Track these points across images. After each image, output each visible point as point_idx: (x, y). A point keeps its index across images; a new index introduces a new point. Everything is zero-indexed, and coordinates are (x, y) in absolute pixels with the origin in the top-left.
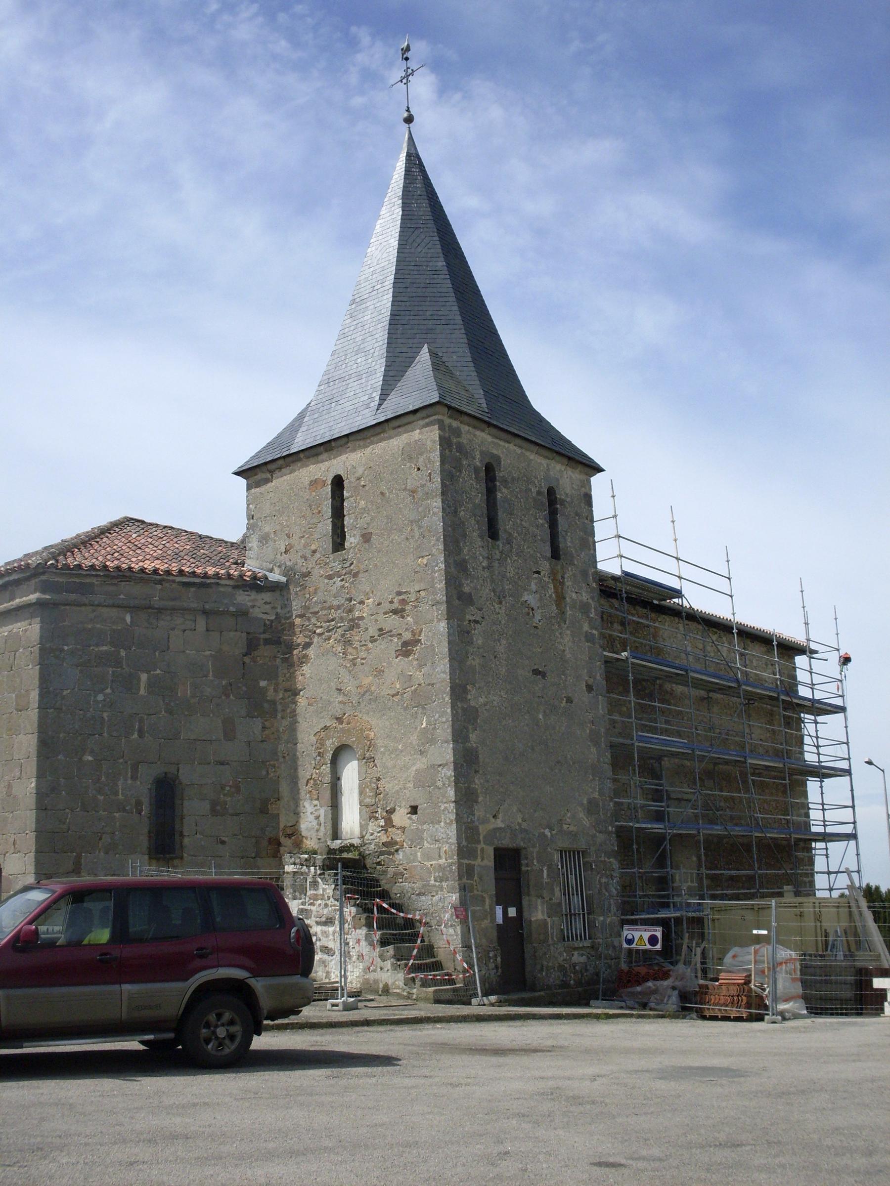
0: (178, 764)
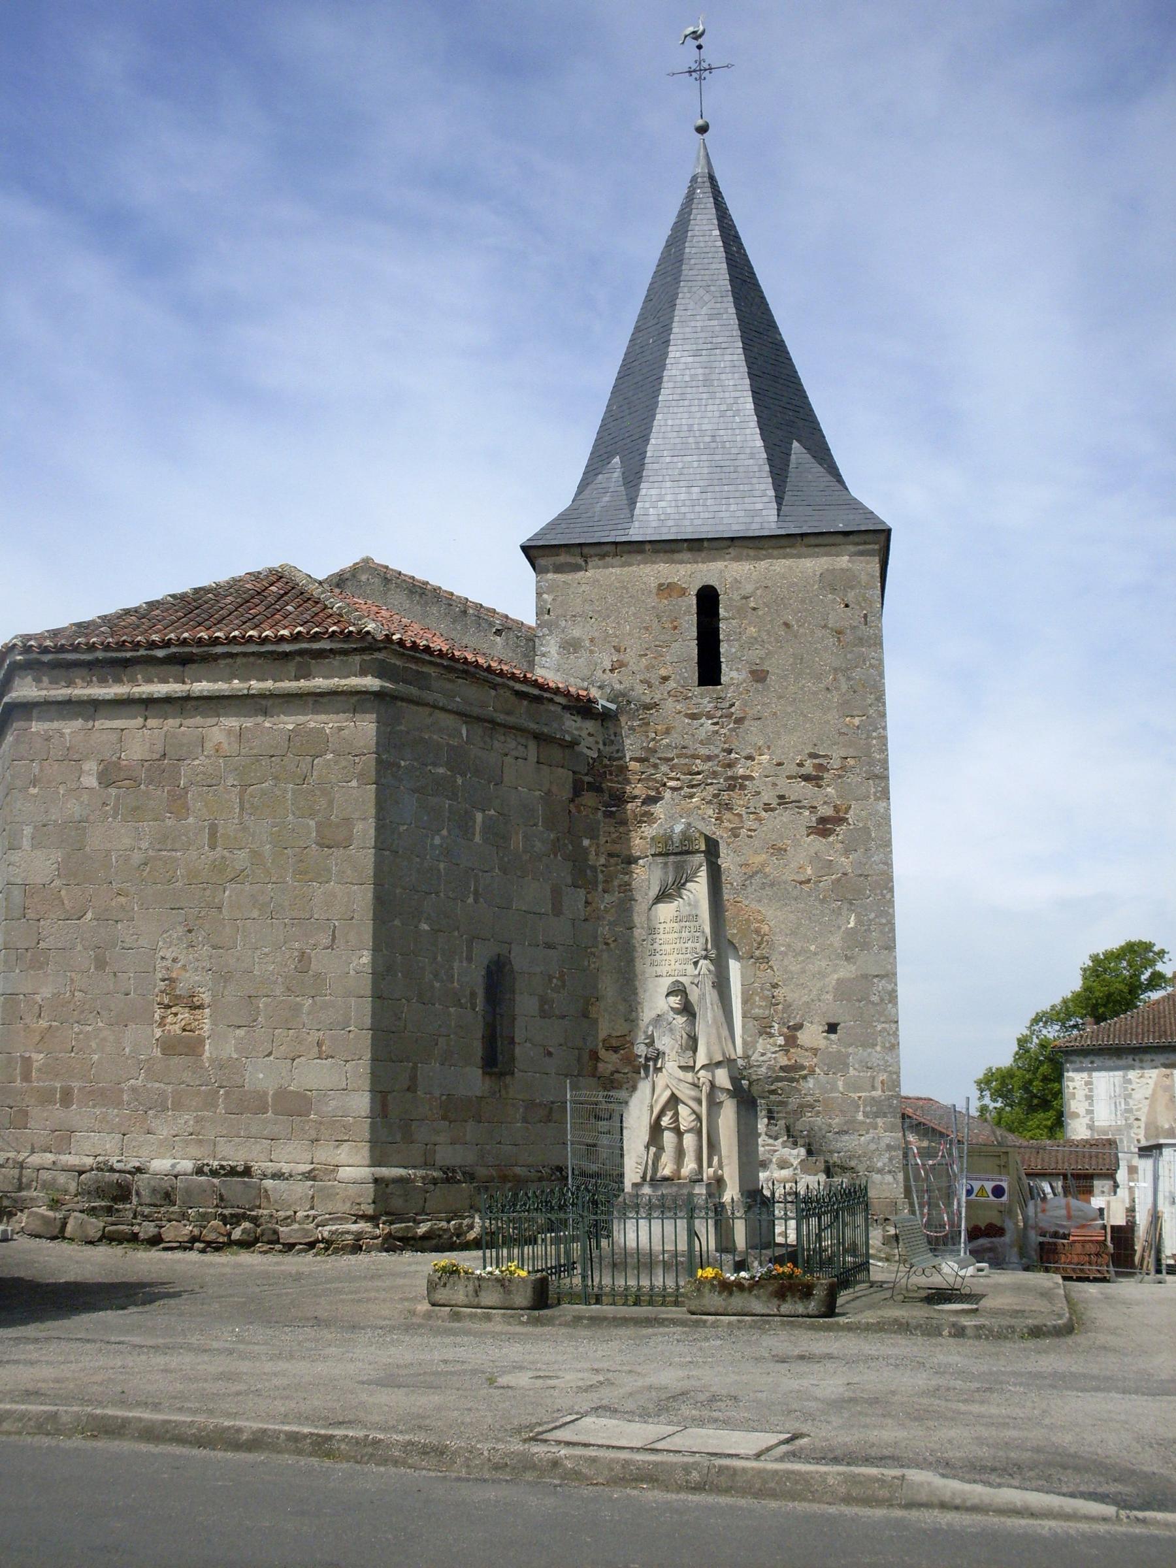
0: (510, 944)
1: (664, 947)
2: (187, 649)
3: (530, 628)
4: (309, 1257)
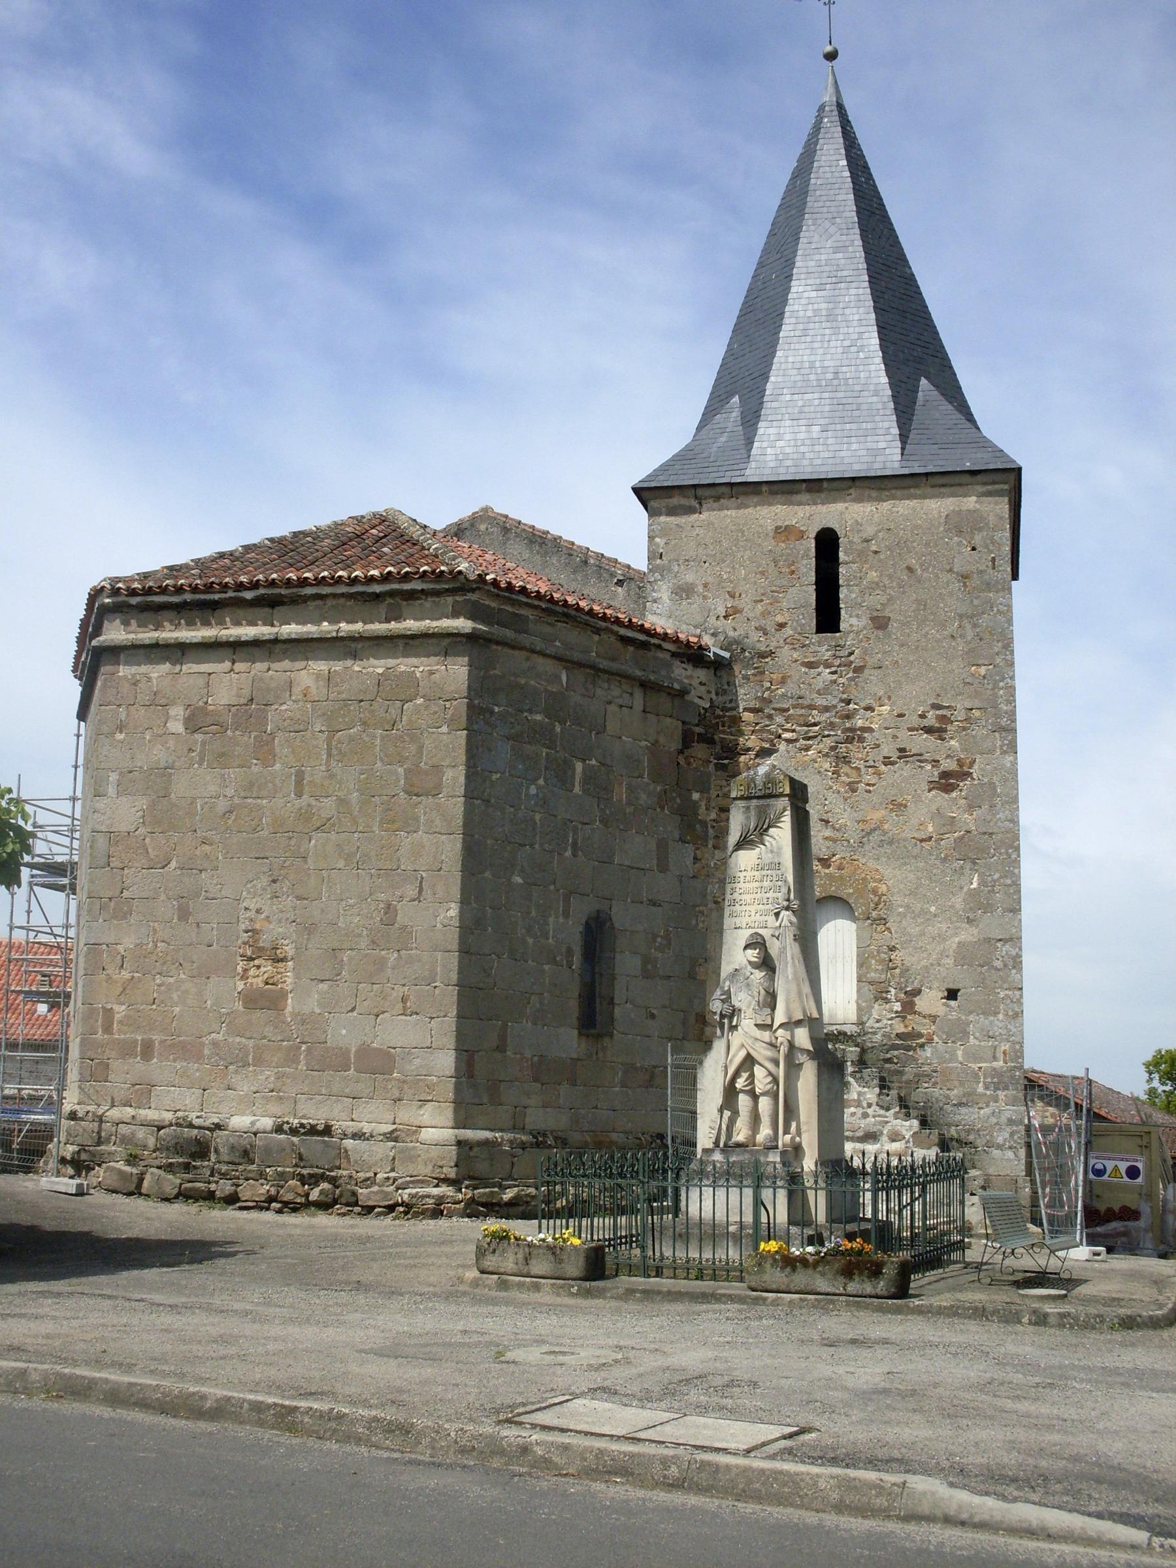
0: (611, 899)
1: (743, 897)
2: (276, 591)
4: (388, 1220)
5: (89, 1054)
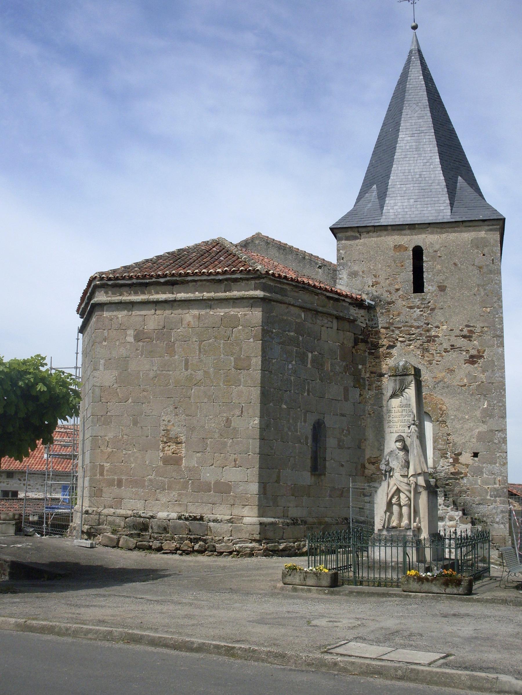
0: (324, 414)
1: (394, 419)
2: (174, 278)
3: (335, 265)
4: (229, 558)
5: (94, 485)
